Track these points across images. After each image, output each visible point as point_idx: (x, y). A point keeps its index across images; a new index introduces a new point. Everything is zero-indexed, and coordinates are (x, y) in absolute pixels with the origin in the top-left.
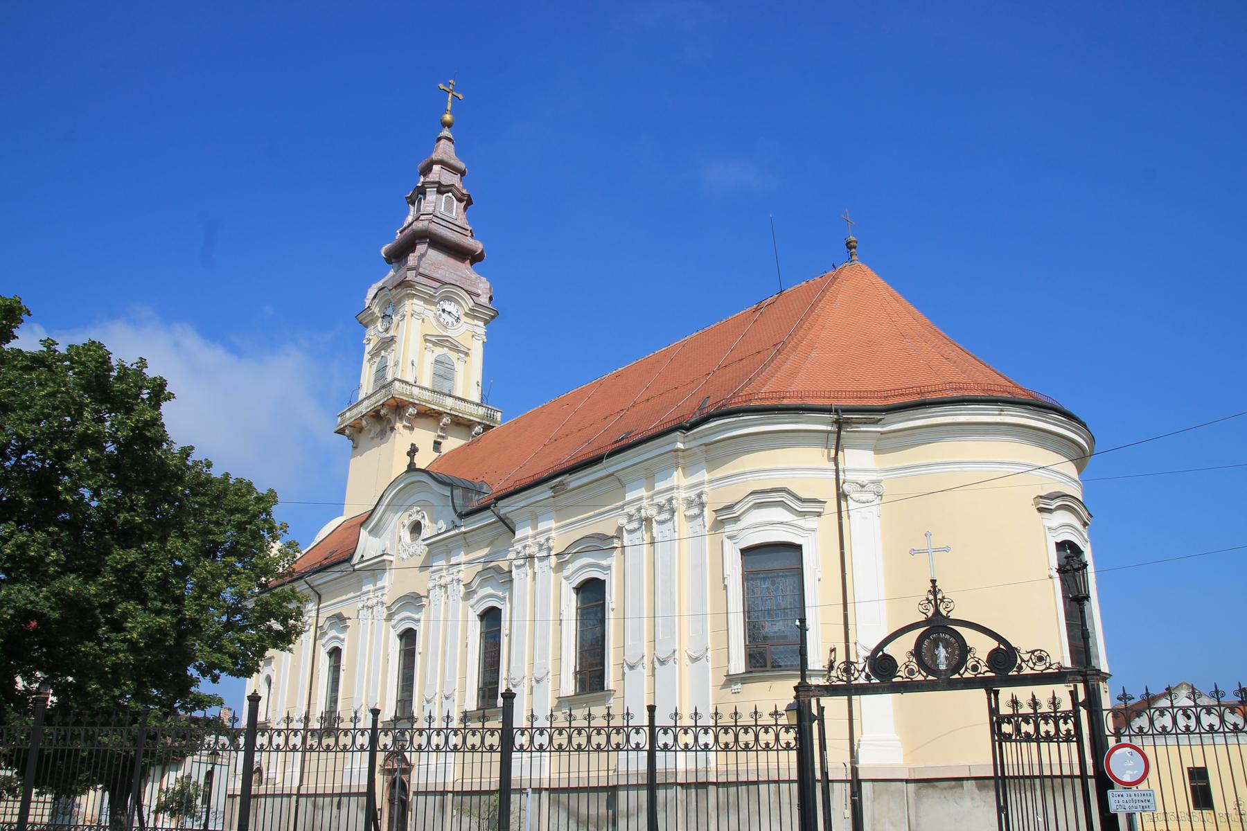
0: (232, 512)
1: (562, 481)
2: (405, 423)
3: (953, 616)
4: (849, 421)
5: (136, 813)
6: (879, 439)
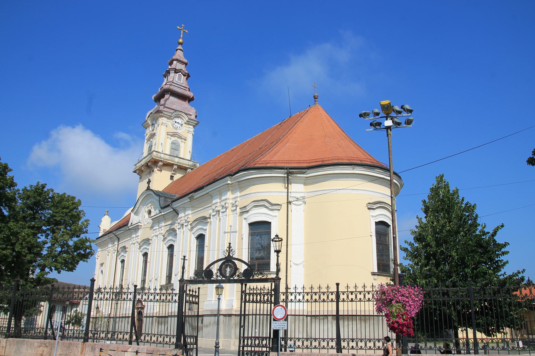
0: (63, 208)
1: (192, 195)
2: (158, 169)
3: (234, 256)
5: (49, 321)
6: (305, 180)
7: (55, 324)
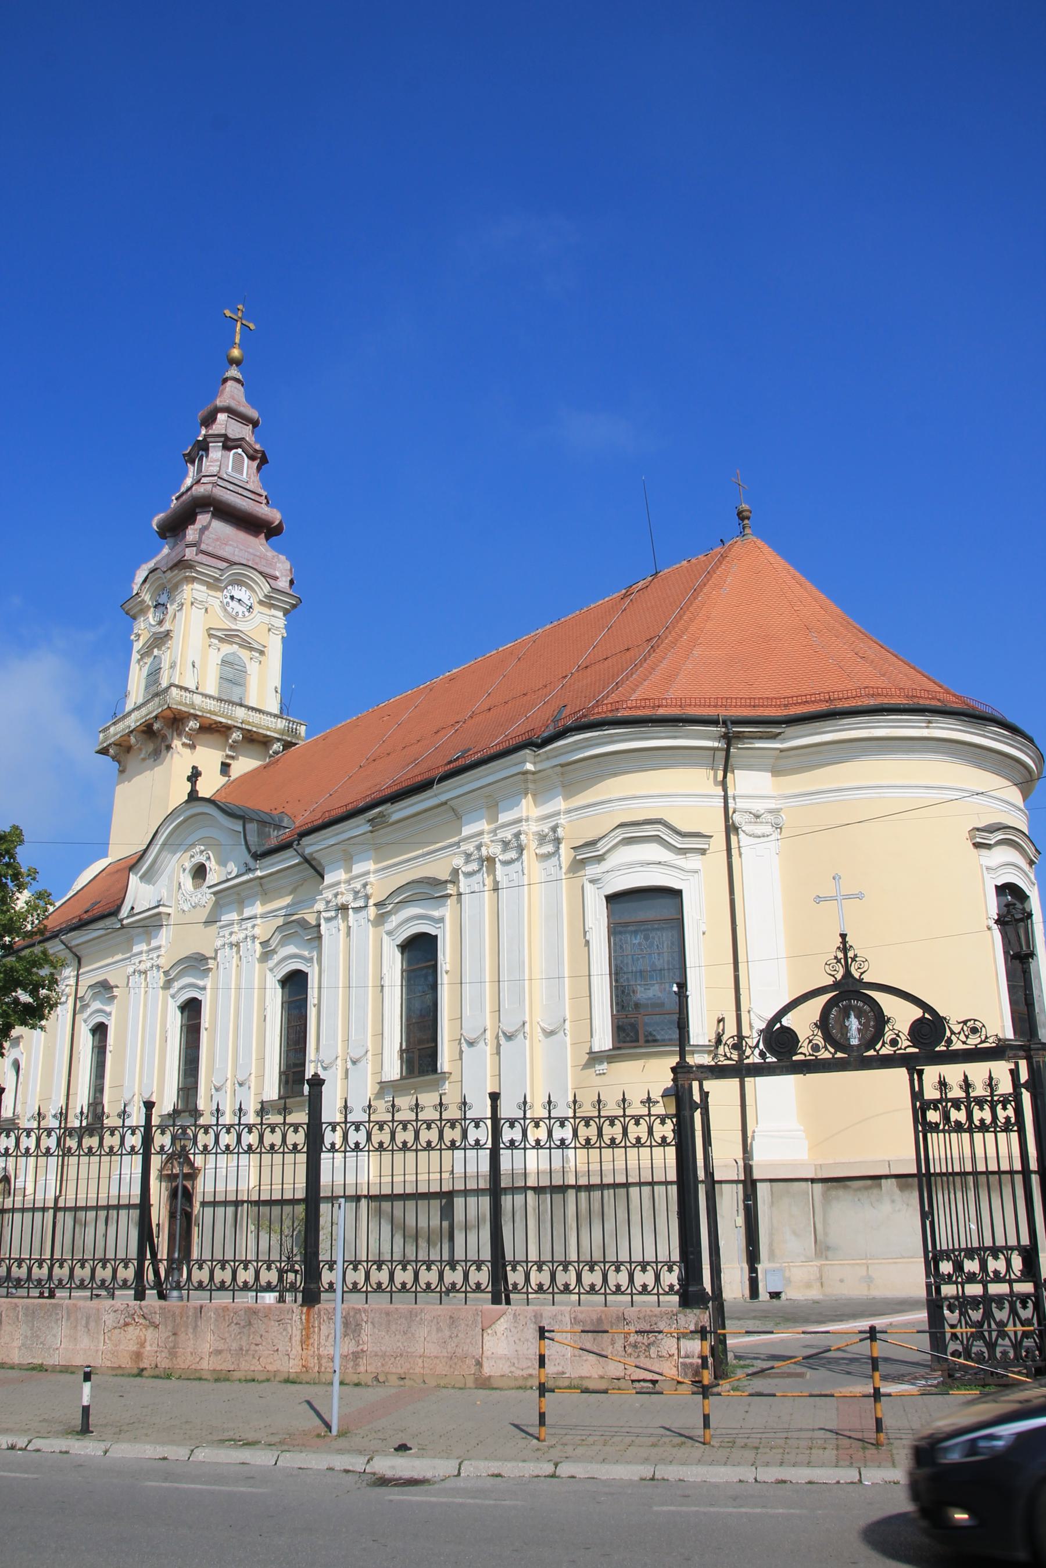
2: (185, 740)
3: (866, 978)
6: (777, 758)
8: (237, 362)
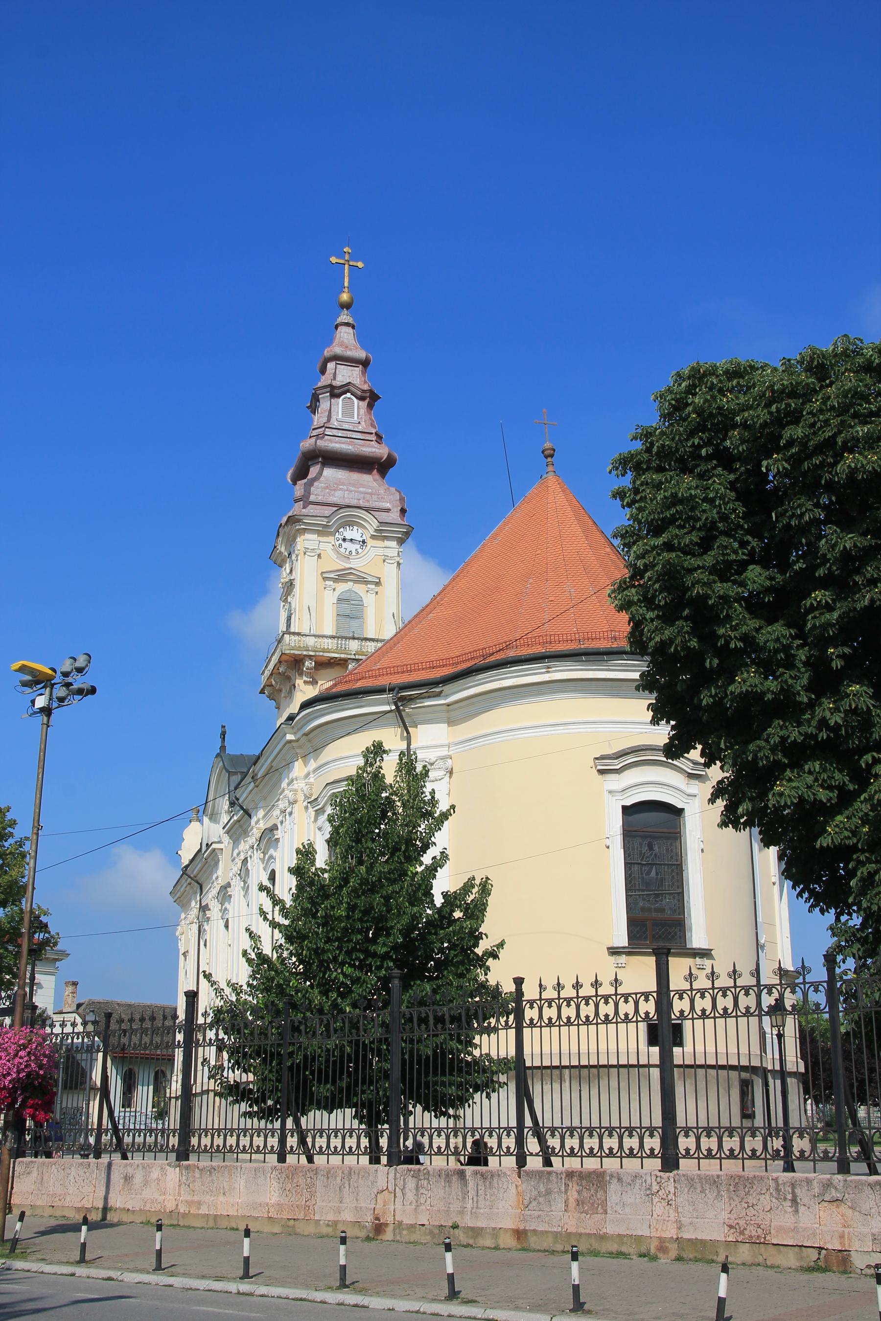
2: (305, 678)
4: (412, 697)
7: (121, 1122)
8: (347, 306)
